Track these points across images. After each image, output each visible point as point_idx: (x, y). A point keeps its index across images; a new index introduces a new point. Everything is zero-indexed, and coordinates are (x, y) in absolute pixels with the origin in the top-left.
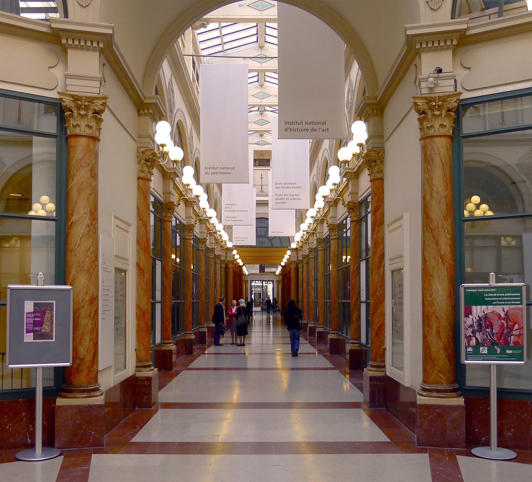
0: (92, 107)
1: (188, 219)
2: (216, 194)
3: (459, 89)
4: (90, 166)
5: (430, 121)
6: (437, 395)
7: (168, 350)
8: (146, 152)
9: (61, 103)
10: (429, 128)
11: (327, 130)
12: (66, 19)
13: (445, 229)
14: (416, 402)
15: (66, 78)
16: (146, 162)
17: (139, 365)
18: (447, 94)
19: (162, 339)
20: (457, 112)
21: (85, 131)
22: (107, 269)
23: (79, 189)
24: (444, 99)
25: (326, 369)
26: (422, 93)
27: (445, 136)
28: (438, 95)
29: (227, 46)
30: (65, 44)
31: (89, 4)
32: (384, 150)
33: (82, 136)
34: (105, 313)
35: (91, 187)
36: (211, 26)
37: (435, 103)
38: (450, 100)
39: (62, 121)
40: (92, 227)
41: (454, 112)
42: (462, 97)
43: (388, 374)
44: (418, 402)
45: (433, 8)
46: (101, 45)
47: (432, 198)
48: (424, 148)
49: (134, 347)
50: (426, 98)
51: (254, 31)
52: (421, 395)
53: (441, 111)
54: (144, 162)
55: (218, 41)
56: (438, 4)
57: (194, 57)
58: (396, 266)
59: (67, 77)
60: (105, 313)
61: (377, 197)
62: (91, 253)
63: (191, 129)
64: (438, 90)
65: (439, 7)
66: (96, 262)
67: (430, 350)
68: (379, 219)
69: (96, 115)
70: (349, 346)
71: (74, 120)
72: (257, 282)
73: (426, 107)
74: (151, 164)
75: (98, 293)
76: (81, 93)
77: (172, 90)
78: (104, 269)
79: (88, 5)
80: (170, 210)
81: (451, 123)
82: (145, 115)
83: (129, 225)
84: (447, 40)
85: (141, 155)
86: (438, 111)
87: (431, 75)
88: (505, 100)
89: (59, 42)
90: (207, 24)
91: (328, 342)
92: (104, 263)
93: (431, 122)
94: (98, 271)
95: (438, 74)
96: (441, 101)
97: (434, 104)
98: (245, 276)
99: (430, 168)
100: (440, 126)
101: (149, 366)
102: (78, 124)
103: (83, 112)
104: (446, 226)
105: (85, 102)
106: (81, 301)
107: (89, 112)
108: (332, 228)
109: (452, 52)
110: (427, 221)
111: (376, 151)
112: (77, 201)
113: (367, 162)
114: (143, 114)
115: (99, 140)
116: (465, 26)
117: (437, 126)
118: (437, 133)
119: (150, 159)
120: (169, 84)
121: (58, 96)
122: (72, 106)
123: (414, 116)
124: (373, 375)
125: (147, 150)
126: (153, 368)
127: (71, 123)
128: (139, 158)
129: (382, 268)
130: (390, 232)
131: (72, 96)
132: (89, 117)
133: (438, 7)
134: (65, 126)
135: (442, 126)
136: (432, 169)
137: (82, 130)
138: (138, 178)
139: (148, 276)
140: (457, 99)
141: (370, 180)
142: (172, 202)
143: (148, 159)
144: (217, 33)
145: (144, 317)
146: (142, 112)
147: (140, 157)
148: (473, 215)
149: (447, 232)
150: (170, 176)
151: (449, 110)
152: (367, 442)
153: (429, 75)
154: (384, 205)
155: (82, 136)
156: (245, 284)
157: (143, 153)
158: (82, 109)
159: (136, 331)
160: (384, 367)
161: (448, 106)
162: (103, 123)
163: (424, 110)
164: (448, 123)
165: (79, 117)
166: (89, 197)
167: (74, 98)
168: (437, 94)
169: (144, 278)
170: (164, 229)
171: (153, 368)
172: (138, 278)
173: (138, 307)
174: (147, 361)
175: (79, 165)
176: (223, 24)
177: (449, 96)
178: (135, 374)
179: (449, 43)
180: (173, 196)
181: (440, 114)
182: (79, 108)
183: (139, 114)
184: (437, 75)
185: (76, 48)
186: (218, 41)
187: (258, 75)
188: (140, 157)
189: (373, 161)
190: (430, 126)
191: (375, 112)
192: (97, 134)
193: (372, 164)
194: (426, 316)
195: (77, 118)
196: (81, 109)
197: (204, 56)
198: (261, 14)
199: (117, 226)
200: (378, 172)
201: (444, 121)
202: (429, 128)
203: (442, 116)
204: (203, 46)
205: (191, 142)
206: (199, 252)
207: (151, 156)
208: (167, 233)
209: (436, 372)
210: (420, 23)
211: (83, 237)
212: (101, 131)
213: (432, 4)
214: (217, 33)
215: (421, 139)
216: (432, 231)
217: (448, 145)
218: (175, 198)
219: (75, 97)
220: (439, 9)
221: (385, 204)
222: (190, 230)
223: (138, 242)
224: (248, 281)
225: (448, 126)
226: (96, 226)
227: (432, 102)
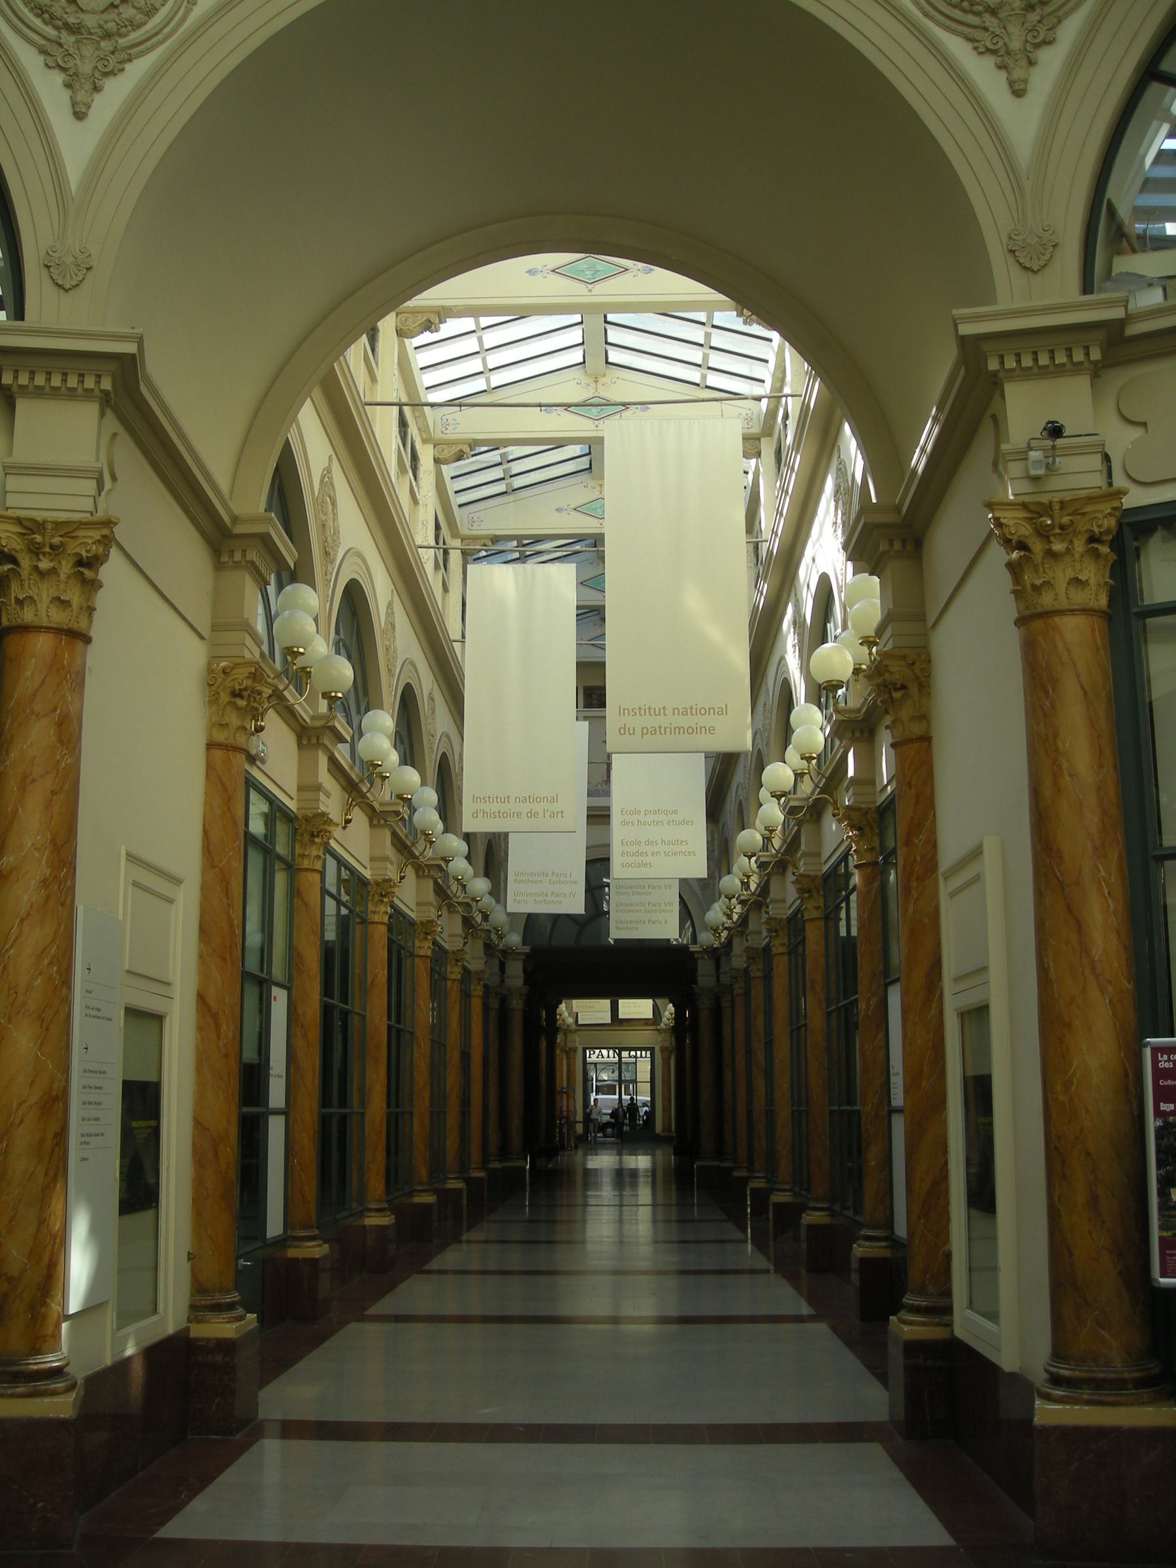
0: (73, 548)
1: (423, 908)
2: (444, 739)
3: (1119, 481)
4: (59, 711)
5: (1041, 570)
6: (1094, 1397)
7: (305, 1260)
8: (233, 672)
11: (560, 815)
13: (1100, 883)
14: (1031, 1420)
15: (6, 474)
16: (233, 700)
17: (198, 1304)
18: (1084, 493)
19: (286, 1225)
20: (1118, 544)
21: (1068, 598)
22: (99, 1010)
23: (24, 778)
24: (1076, 505)
25: (799, 1319)
27: (1085, 611)
28: (1057, 498)
29: (497, 379)
31: (81, 281)
32: (929, 655)
33: (38, 629)
34: (88, 1143)
35: (58, 770)
36: (451, 327)
37: (1052, 520)
38: (1096, 511)
40: (56, 887)
41: (1108, 543)
42: (1128, 502)
43: (959, 1332)
44: (1038, 1420)
45: (1028, 265)
46: (106, 384)
47: (1059, 791)
48: (1030, 648)
49: (186, 1245)
50: (1024, 506)
51: (575, 336)
52: (1048, 1398)
53: (1071, 541)
54: (227, 699)
55: (475, 365)
57: (404, 407)
58: (971, 999)
60: (88, 1143)
61: (913, 791)
62: (50, 963)
63: (390, 605)
64: (1056, 483)
65: (1045, 265)
66: (65, 991)
67: (1071, 1254)
68: (922, 858)
69: (82, 569)
70: (859, 1246)
71: (22, 585)
72: (605, 1052)
73: (1026, 530)
74: (247, 705)
75: (68, 1080)
76: (40, 513)
77: (330, 497)
78: (88, 1011)
79: (77, 285)
80: (318, 836)
81: (1103, 576)
82: (237, 565)
83: (177, 881)
84: (1090, 348)
85: (219, 680)
86: (1062, 541)
87: (1034, 443)
90: (441, 322)
91: (803, 1234)
92: (90, 992)
93: (30, 588)
94: (68, 1018)
95: (1054, 441)
96: (1068, 515)
97: (1049, 522)
98: (565, 1035)
99: (1047, 703)
100: (1069, 584)
101: (231, 1306)
102: (31, 598)
103: (44, 564)
104: (1103, 873)
105: (52, 536)
106: (15, 1104)
107: (64, 563)
108: (806, 887)
110: (1048, 862)
111: (904, 657)
112: (15, 812)
113: (882, 688)
114: (230, 563)
115: (87, 640)
116: (1118, 313)
117: (1061, 586)
118: (1064, 604)
119: (246, 689)
120: (322, 481)
122: (18, 548)
123: (998, 556)
124: (913, 1337)
125: (236, 666)
126: (240, 1311)
127: (13, 595)
128: (213, 688)
129: (934, 1006)
130: (953, 895)
131: (19, 521)
132: (63, 577)
133: (1042, 263)
135: (1076, 582)
136: (1053, 706)
137: (43, 611)
138: (207, 745)
139: (230, 1034)
140: (1114, 509)
141: (891, 741)
142: (324, 814)
143: (240, 690)
144: (470, 344)
145: (216, 1155)
146: (227, 560)
147: (218, 683)
149: (1106, 892)
150: (318, 740)
151: (1093, 539)
153: (1029, 443)
154: (934, 815)
155: (38, 629)
156: (568, 1059)
157: (225, 672)
158: (44, 554)
159: (193, 1200)
160: (948, 1310)
161: (78, 550)
162: (101, 593)
163: (1023, 539)
164: (1094, 574)
165: (35, 576)
166: (51, 800)
168: (1054, 494)
169: (219, 1038)
170: (299, 894)
171: (240, 1311)
172: (202, 1040)
173: (199, 1124)
174: (224, 1291)
175: (28, 711)
176: (485, 321)
177: (1090, 500)
178: (187, 1329)
179: (1078, 356)
180: (328, 795)
181: (1068, 551)
182: (36, 551)
183: (219, 566)
184: (1049, 443)
186: (475, 365)
187: (590, 454)
188: (218, 683)
189: (898, 686)
190: (1042, 584)
191: (897, 546)
192: (82, 624)
193: (897, 695)
194: (1056, 1149)
195: (30, 579)
197: (432, 405)
198: (590, 291)
199: (136, 884)
200: (913, 718)
201: (1080, 570)
203: (1073, 555)
204: (429, 379)
205: (389, 640)
206: (413, 963)
207: (249, 682)
208: (306, 904)
209: (1089, 1325)
210: (995, 303)
211: (28, 915)
212: (96, 615)
213: (59, 274)
214: (470, 344)
215: (1020, 622)
216: (1063, 889)
217: (1098, 639)
218: (332, 803)
219: (27, 524)
221: (937, 813)
222: (382, 895)
223: (203, 931)
224: (575, 1050)
225: (1093, 582)
226: (69, 883)
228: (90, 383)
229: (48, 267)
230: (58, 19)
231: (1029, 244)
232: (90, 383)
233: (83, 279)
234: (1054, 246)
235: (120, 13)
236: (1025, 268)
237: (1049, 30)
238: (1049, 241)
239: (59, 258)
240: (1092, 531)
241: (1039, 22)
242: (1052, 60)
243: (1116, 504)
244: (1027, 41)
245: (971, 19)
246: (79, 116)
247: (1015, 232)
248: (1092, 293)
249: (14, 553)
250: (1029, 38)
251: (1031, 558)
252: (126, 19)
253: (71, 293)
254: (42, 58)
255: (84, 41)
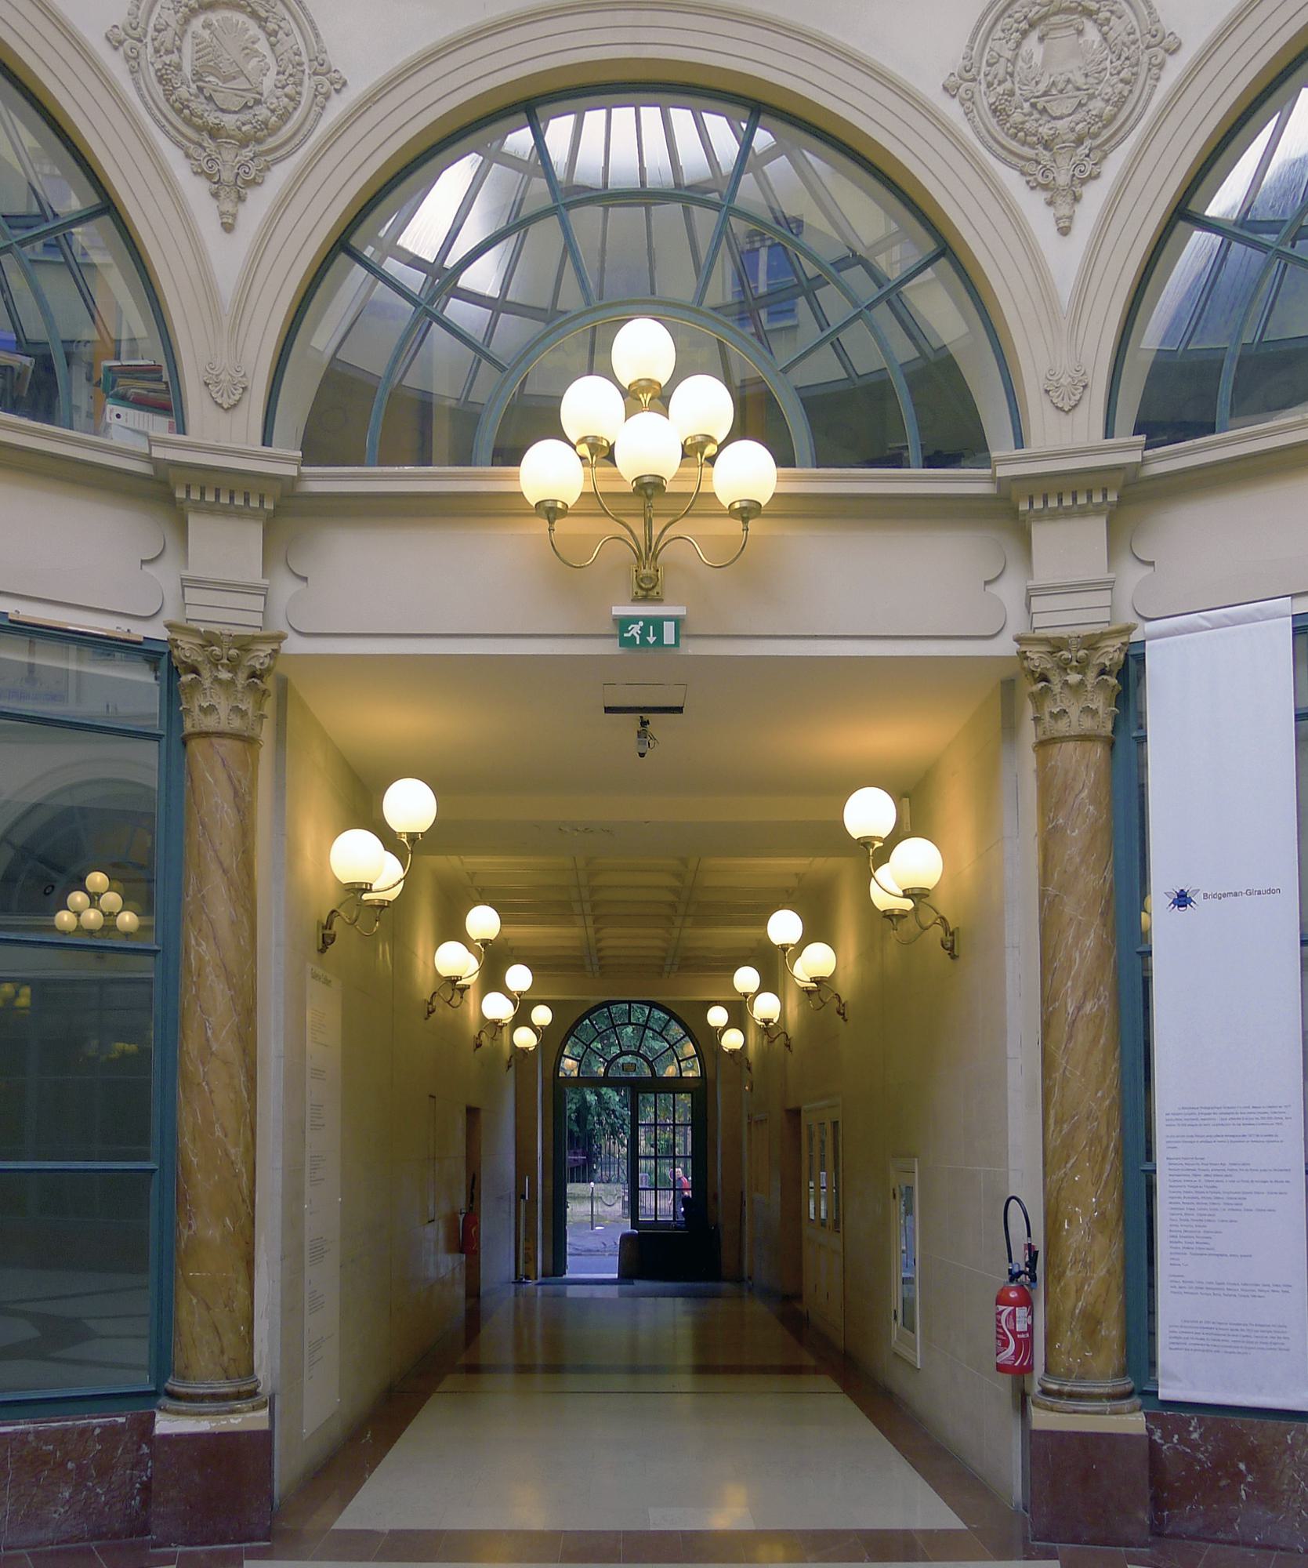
9: (170, 653)
10: (1055, 717)
12: (181, 437)
15: (183, 587)
26: (1035, 625)
30: (182, 502)
31: (1079, 401)
38: (1107, 646)
39: (172, 696)
56: (1076, 392)
59: (186, 583)
79: (1076, 405)
88: (41, 641)
89: (169, 499)
93: (212, 697)
105: (230, 649)
107: (240, 674)
109: (1105, 521)
117: (1074, 712)
118: (224, 726)
121: (163, 634)
131: (1046, 641)
132: (239, 687)
133: (1073, 403)
134: (181, 708)
140: (1122, 644)
148: (50, 924)
152: (258, 1432)
158: (223, 665)
161: (1101, 660)
164: (1100, 702)
165: (1066, 691)
167: (1053, 646)
181: (1082, 683)
182: (215, 662)
185: (212, 510)
196: (220, 667)
202: (1055, 717)
213: (1059, 396)
220: (1077, 409)
227: (213, 645)
228: (1097, 499)
229: (207, 385)
230: (1034, 135)
231: (1062, 385)
232: (1097, 499)
233: (1081, 397)
234: (1085, 387)
235: (1090, 110)
236: (1057, 407)
237: (1095, 164)
238: (240, 382)
239: (217, 375)
240: (254, 667)
241: (1088, 156)
242: (1095, 196)
243: (1124, 639)
244: (1074, 175)
245: (1026, 151)
246: (1064, 231)
247: (1051, 373)
248: (1113, 437)
249: (196, 664)
250: (1077, 172)
251: (1050, 688)
252: (1096, 116)
253: (1071, 413)
254: (1024, 179)
255: (226, 145)
